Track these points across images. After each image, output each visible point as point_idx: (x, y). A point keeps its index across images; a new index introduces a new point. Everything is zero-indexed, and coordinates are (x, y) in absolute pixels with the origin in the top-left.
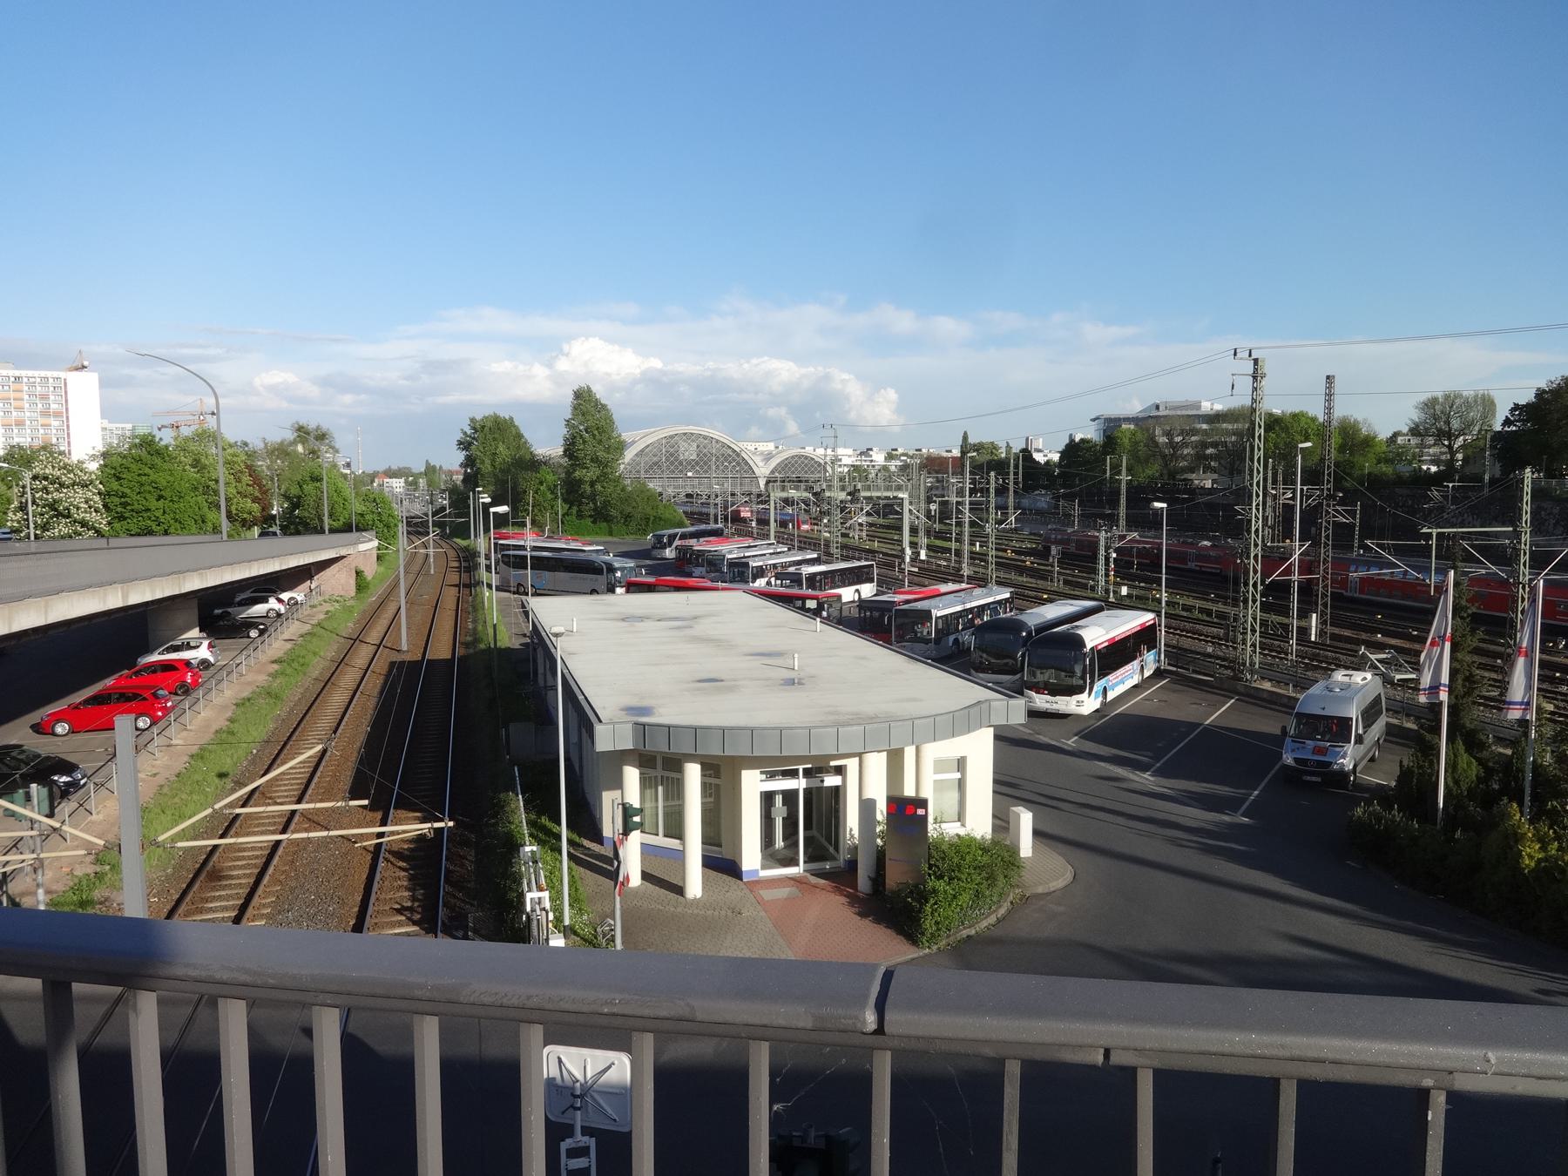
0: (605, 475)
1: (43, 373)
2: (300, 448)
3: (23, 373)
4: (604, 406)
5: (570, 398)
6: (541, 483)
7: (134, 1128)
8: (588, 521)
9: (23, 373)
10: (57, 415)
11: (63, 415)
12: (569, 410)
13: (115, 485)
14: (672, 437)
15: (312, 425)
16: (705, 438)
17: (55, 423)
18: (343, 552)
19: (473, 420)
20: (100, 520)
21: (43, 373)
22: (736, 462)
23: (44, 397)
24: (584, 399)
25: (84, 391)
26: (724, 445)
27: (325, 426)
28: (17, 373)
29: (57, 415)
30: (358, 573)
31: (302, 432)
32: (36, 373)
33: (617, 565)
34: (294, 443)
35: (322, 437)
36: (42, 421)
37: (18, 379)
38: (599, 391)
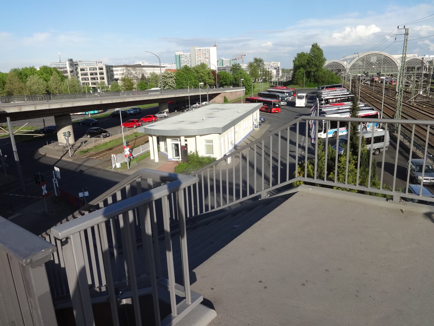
0: (318, 70)
1: (205, 48)
2: (255, 64)
3: (201, 48)
4: (320, 49)
5: (311, 47)
6: (300, 72)
7: (202, 263)
8: (312, 83)
9: (201, 48)
10: (208, 58)
11: (209, 58)
12: (310, 50)
13: (178, 77)
14: (368, 55)
15: (258, 58)
16: (380, 55)
17: (207, 60)
18: (221, 92)
19: (297, 54)
20: (175, 86)
21: (205, 48)
22: (388, 62)
23: (205, 54)
24: (315, 48)
25: (213, 51)
26: (386, 57)
27: (261, 58)
28: (200, 48)
29: (208, 58)
30: (225, 97)
31: (256, 60)
32: (204, 48)
33: (280, 96)
34: (254, 63)
35: (261, 61)
36: (205, 60)
37: (200, 50)
38: (321, 46)
